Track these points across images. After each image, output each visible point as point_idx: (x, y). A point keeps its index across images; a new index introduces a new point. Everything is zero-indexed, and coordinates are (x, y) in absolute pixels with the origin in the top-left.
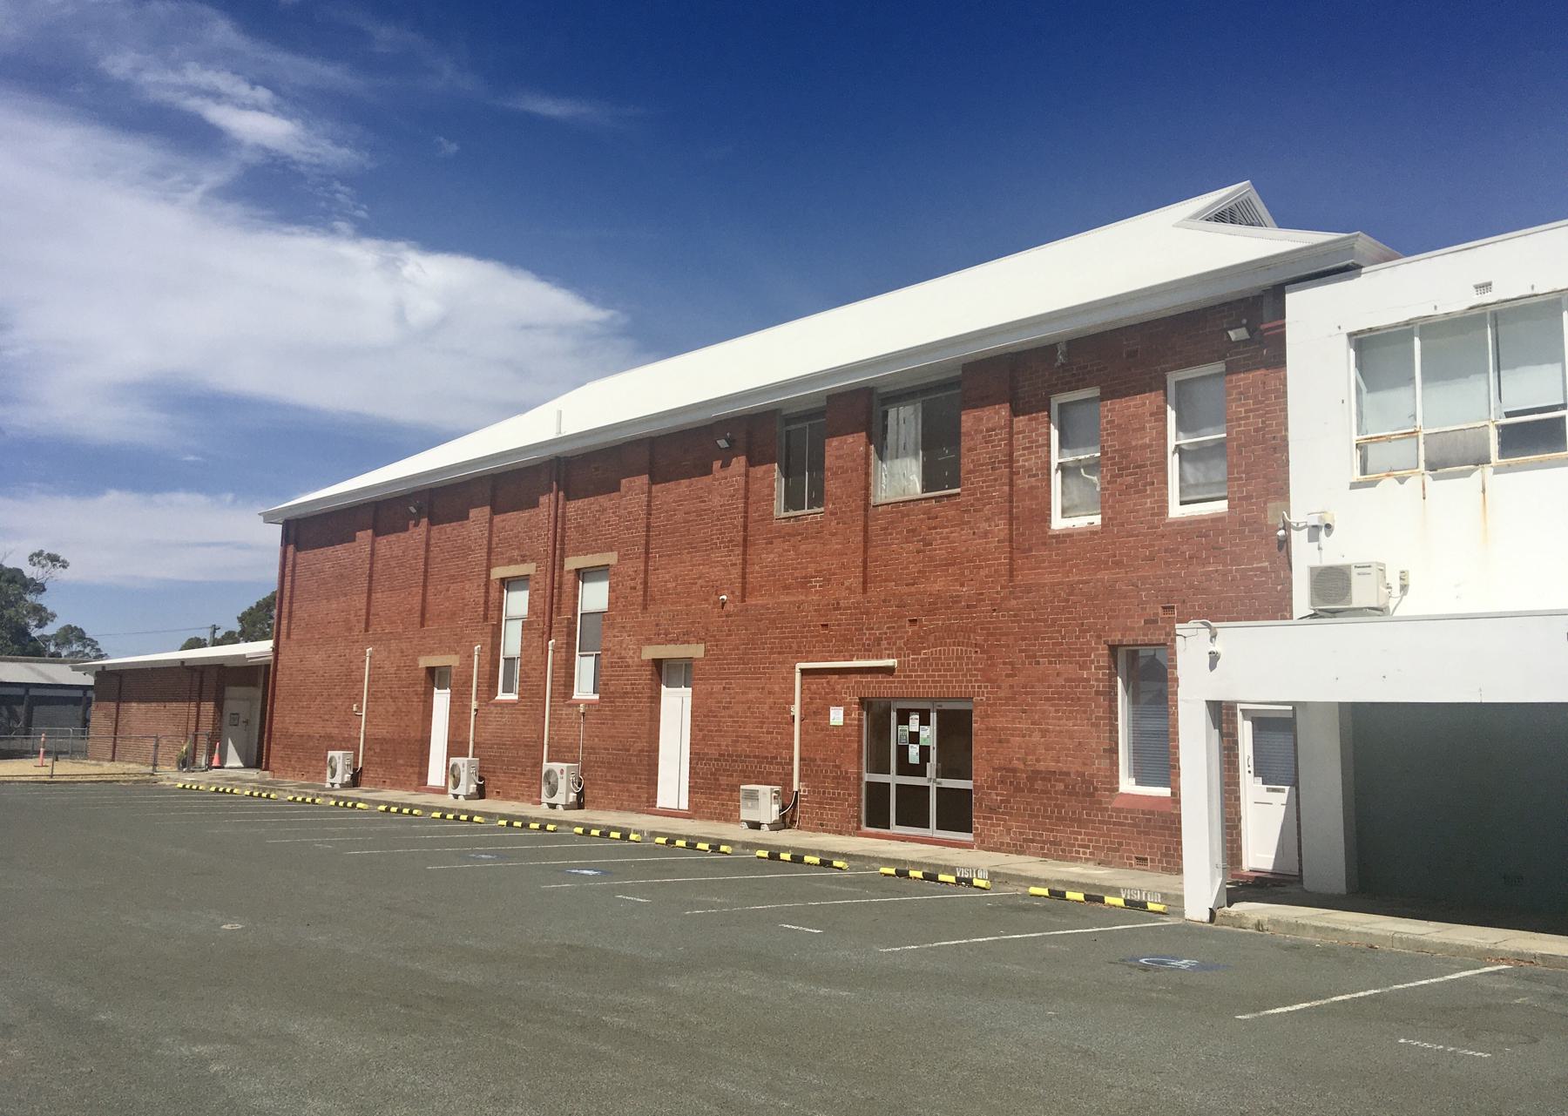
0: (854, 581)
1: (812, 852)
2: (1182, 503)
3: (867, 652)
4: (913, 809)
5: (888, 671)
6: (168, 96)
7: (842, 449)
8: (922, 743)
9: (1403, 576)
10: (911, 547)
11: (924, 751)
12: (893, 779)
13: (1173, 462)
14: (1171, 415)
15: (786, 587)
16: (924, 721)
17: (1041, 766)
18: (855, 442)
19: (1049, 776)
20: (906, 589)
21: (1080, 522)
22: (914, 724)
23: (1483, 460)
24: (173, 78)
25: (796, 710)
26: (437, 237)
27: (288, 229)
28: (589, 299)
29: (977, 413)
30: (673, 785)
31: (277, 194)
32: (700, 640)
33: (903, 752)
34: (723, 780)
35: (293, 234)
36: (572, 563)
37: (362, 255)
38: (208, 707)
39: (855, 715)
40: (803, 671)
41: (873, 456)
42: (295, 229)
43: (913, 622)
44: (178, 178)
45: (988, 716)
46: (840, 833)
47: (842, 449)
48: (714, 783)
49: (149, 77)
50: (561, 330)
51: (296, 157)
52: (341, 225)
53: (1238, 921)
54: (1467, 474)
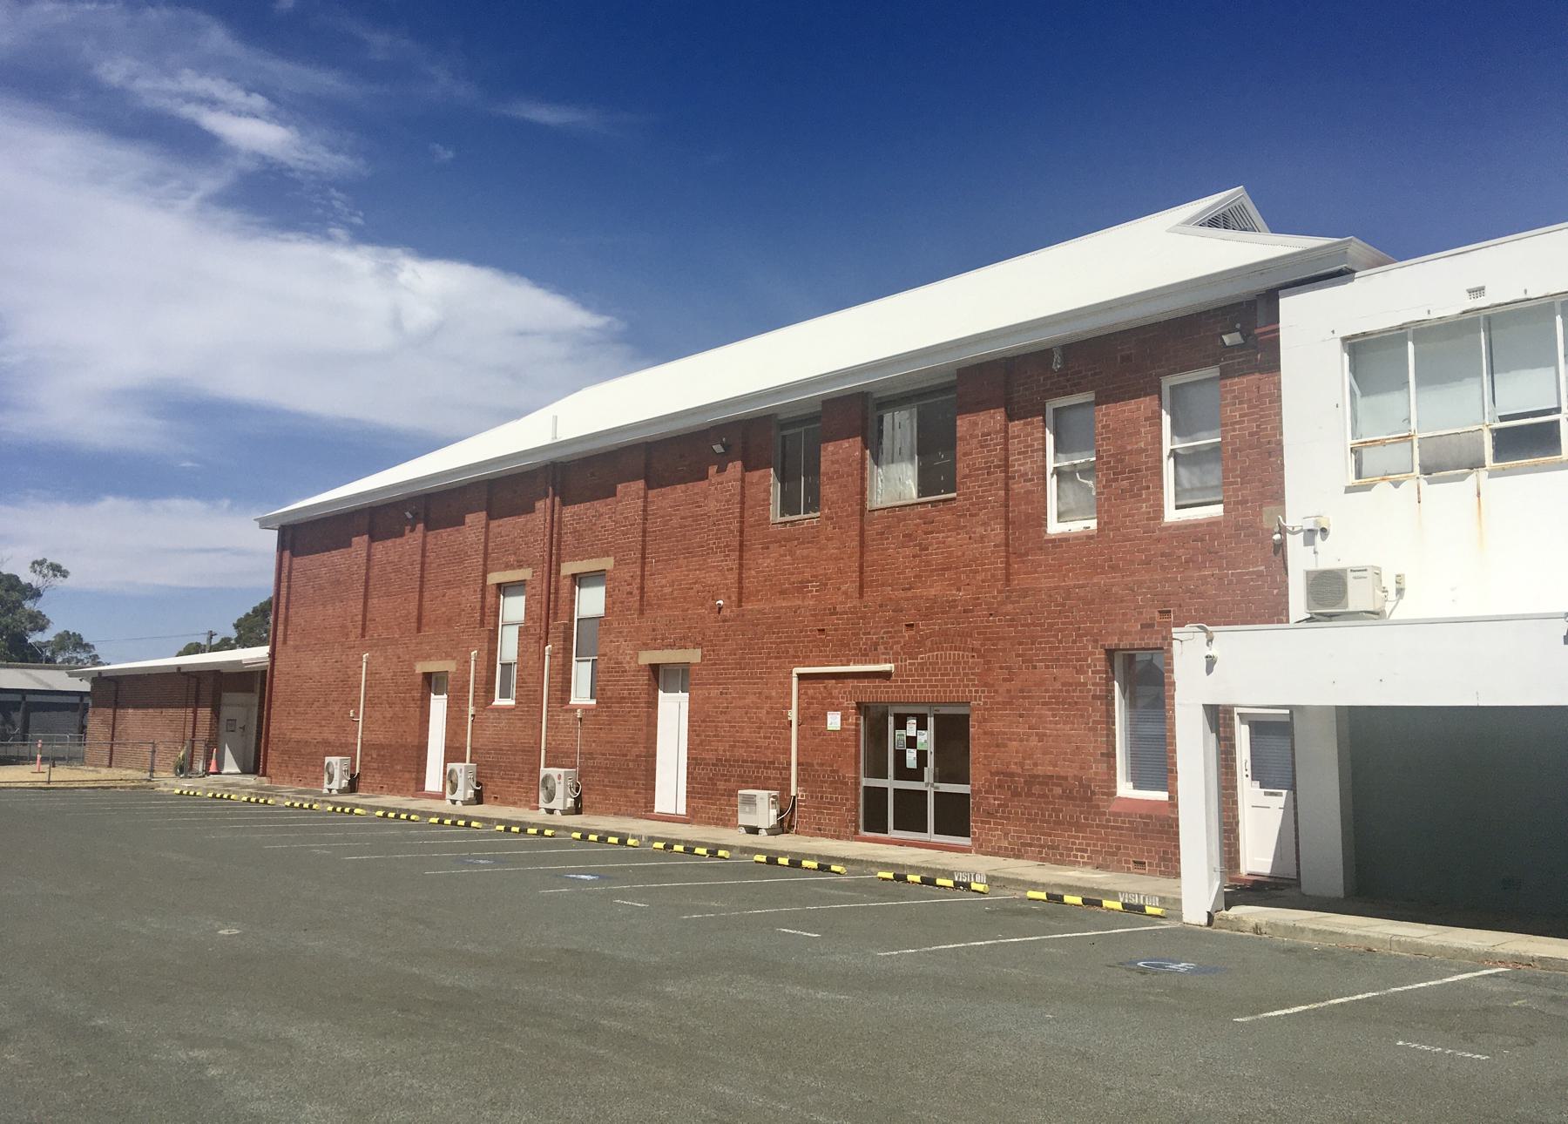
0: (851, 586)
1: (810, 857)
2: (1177, 507)
3: (864, 657)
4: (910, 814)
5: (886, 675)
6: (163, 103)
7: (837, 454)
8: (919, 747)
9: (1399, 579)
10: (908, 551)
11: (922, 756)
12: (891, 784)
13: (1168, 466)
14: (1166, 419)
15: (781, 593)
16: (922, 726)
17: (1040, 770)
18: (850, 447)
19: (1048, 780)
20: (902, 594)
21: (1076, 526)
22: (911, 728)
23: (1478, 464)
24: (167, 84)
25: (793, 715)
26: (432, 244)
27: (284, 236)
28: (586, 306)
29: (972, 417)
30: (671, 790)
31: (272, 200)
32: (697, 645)
33: (900, 756)
34: (721, 785)
35: (287, 240)
36: (568, 568)
37: (359, 262)
38: (205, 713)
39: (852, 720)
40: (801, 677)
41: (869, 462)
42: (292, 236)
43: (910, 626)
44: (175, 184)
45: (985, 720)
46: (838, 838)
47: (837, 454)
48: (712, 787)
49: (142, 85)
50: (556, 337)
51: (291, 163)
52: (338, 232)
53: (1235, 924)
54: (1462, 478)
